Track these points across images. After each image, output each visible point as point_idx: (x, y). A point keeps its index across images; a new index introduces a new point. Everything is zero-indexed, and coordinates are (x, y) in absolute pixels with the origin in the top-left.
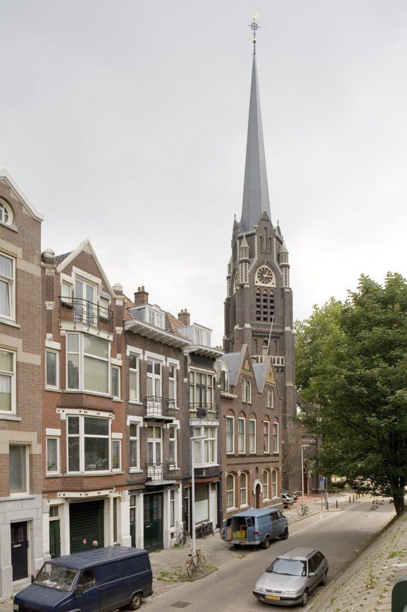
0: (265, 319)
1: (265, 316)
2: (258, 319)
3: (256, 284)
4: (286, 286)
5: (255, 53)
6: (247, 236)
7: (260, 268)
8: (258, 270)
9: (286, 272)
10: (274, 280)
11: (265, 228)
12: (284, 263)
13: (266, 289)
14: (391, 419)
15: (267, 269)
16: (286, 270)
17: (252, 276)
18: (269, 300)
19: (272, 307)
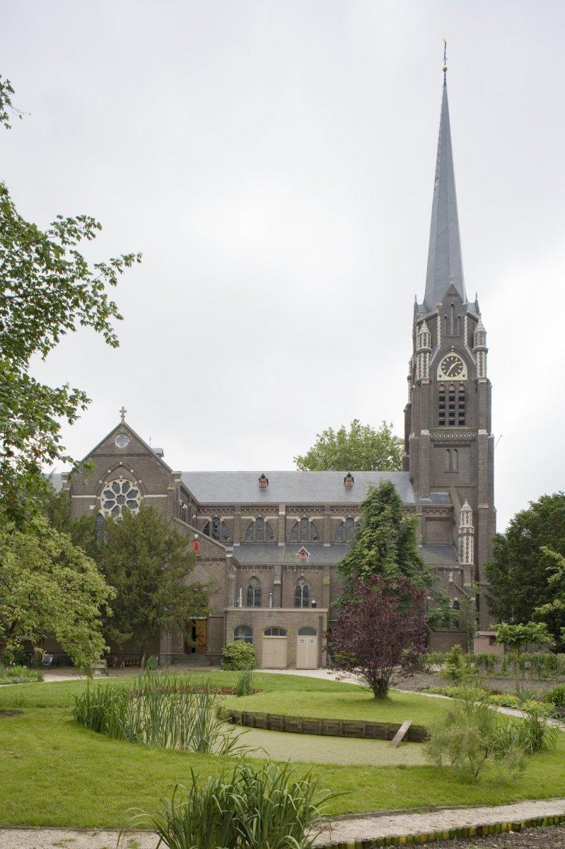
0: (452, 423)
1: (452, 418)
2: (442, 423)
3: (439, 379)
4: (481, 375)
5: (445, 84)
6: (427, 320)
7: (445, 358)
8: (443, 359)
9: (481, 358)
10: (465, 371)
11: (452, 305)
12: (479, 346)
13: (453, 384)
14: (71, 630)
15: (455, 358)
16: (481, 354)
17: (433, 369)
18: (447, 398)
19: (462, 415)
